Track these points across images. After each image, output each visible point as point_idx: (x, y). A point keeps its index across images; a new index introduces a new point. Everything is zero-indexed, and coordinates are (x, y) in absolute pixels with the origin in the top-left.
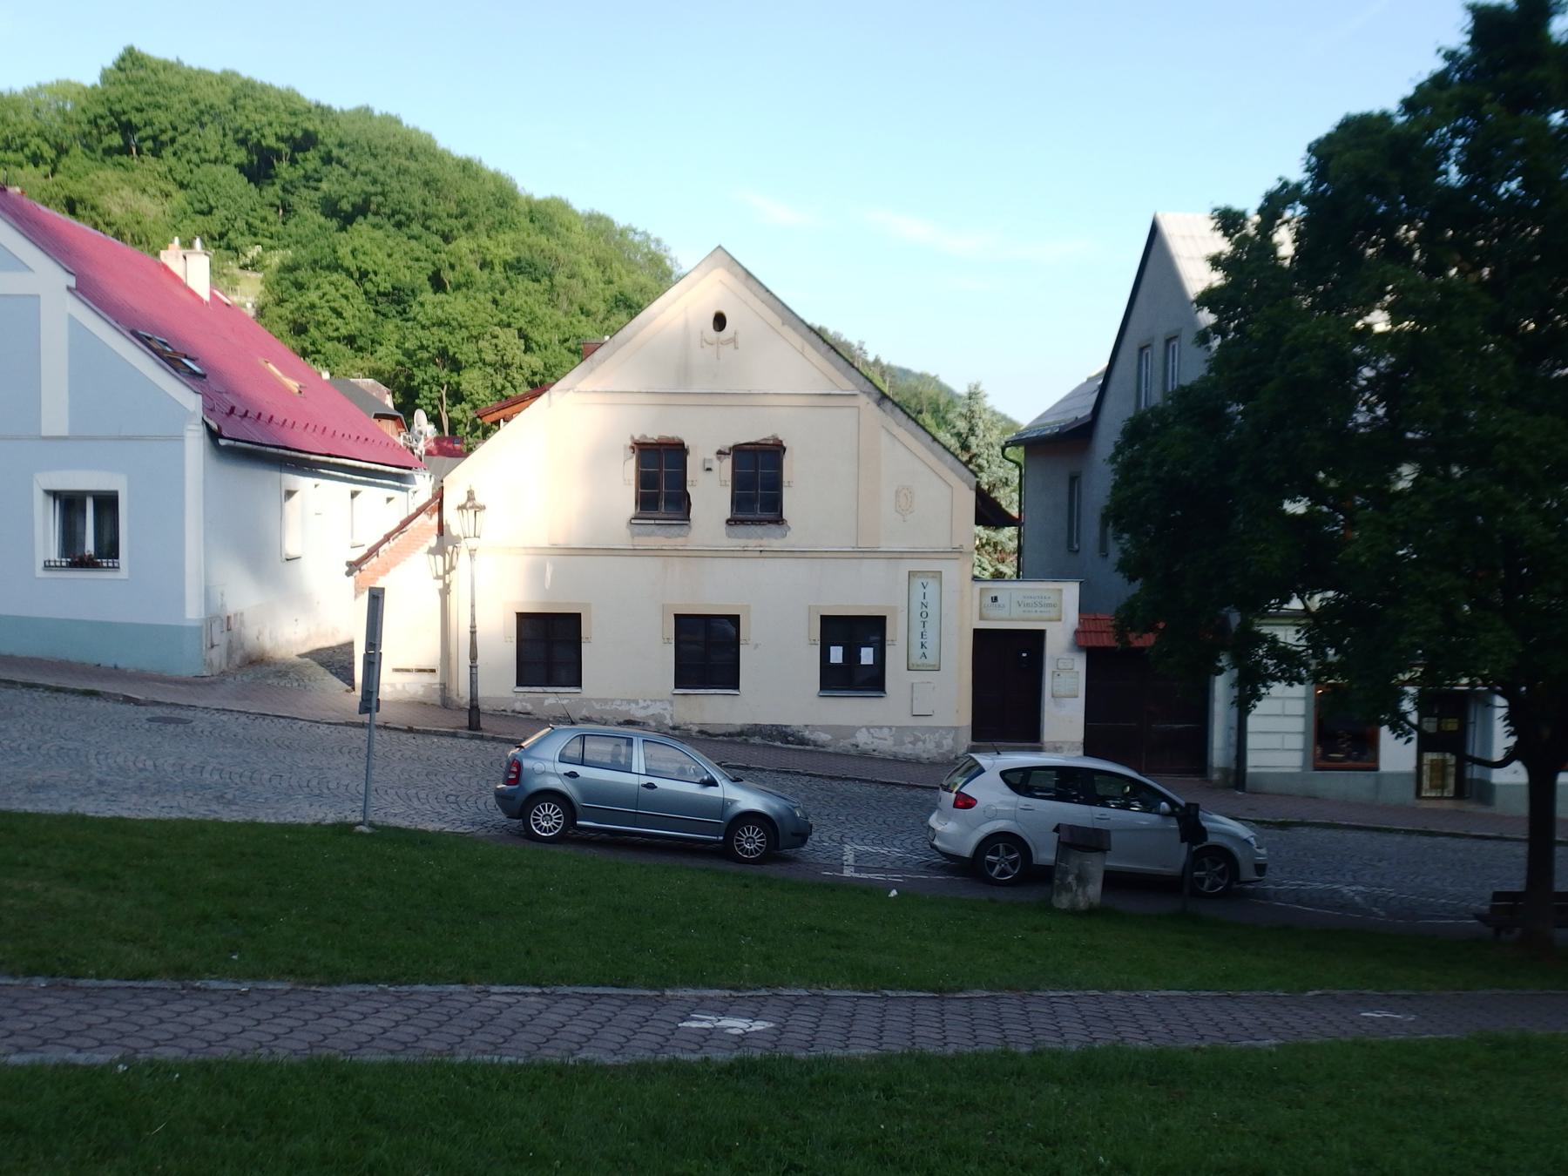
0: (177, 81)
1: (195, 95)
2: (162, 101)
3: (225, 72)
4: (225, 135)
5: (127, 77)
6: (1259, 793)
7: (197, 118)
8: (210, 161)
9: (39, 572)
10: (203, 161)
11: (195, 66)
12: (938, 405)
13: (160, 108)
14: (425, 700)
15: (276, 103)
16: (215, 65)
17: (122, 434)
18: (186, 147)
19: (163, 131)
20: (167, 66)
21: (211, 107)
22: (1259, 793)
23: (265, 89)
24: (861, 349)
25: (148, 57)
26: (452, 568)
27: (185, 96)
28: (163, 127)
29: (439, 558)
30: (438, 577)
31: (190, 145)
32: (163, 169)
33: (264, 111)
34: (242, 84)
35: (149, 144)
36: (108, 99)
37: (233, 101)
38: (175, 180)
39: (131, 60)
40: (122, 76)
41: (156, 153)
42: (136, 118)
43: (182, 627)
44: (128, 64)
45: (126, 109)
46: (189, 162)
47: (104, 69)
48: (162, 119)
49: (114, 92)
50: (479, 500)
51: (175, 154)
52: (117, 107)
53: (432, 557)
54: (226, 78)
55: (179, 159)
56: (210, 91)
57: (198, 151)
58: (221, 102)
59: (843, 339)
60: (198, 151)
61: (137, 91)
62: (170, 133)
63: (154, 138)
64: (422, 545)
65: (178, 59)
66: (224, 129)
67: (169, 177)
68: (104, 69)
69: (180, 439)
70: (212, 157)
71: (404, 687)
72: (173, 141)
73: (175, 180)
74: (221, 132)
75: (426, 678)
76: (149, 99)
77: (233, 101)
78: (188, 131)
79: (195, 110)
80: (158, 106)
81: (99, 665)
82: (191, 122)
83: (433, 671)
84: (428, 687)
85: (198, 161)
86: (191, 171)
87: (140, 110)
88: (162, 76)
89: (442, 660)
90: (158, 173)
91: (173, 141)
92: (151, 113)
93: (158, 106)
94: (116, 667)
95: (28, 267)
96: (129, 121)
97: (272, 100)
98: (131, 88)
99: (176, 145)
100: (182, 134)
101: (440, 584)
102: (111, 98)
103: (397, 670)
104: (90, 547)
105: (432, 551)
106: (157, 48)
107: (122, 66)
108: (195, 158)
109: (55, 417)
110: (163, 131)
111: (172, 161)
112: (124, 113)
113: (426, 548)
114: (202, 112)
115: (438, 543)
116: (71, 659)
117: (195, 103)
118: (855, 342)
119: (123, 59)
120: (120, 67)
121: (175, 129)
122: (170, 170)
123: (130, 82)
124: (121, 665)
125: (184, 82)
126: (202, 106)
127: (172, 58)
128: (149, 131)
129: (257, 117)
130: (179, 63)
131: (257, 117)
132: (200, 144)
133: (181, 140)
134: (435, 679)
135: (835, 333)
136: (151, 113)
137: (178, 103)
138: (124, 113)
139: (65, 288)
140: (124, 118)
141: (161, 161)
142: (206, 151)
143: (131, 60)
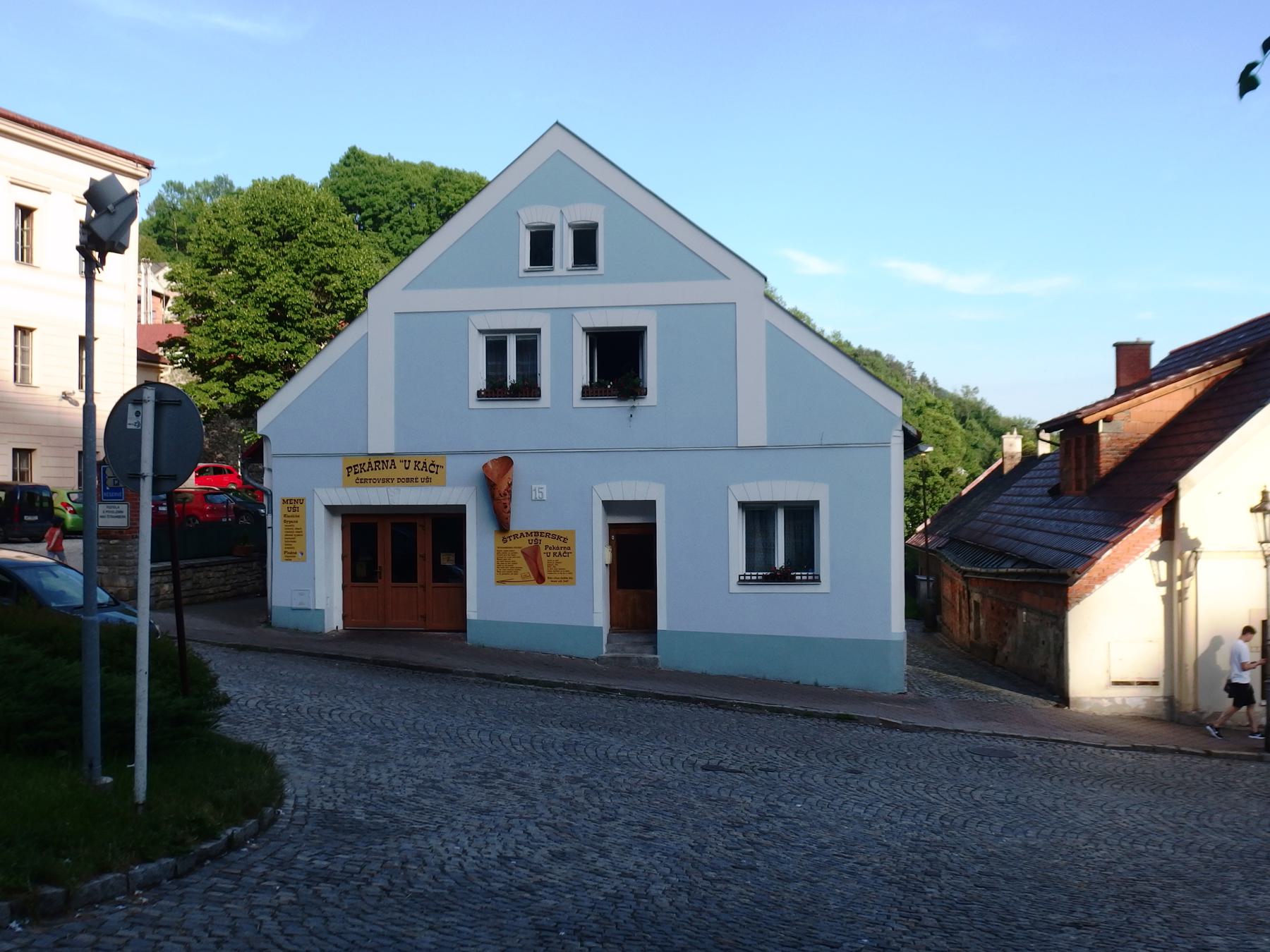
0: (390, 172)
1: (406, 182)
2: (380, 188)
3: (423, 163)
4: (429, 212)
5: (352, 170)
6: (229, 646)
7: (408, 200)
8: (420, 233)
9: (734, 587)
10: (414, 233)
11: (402, 160)
12: (980, 412)
13: (378, 193)
14: (1149, 714)
15: (470, 185)
16: (416, 158)
17: (824, 443)
18: (400, 222)
19: (382, 211)
20: (380, 161)
21: (419, 190)
22: (229, 646)
23: (460, 174)
24: (910, 368)
25: (368, 155)
26: (1186, 574)
27: (398, 183)
28: (382, 208)
29: (1163, 565)
30: (1160, 584)
31: (403, 221)
32: (382, 240)
33: (460, 191)
34: (441, 171)
35: (370, 222)
36: (338, 188)
37: (436, 185)
38: (391, 248)
39: (354, 157)
40: (348, 169)
41: (376, 228)
42: (360, 202)
43: (888, 642)
44: (352, 161)
45: (352, 195)
46: (402, 234)
47: (333, 166)
48: (381, 201)
49: (345, 182)
50: (1257, 501)
51: (391, 228)
52: (346, 194)
53: (1154, 562)
54: (426, 167)
55: (395, 232)
56: (415, 177)
57: (409, 225)
58: (426, 186)
59: (895, 360)
60: (409, 225)
61: (361, 181)
62: (387, 213)
63: (374, 217)
64: (1143, 551)
65: (389, 154)
66: (429, 207)
67: (387, 246)
68: (333, 166)
69: (886, 445)
70: (421, 229)
71: (1124, 700)
72: (388, 218)
73: (391, 248)
74: (427, 210)
75: (1148, 691)
76: (370, 187)
77: (436, 185)
78: (400, 211)
79: (406, 193)
80: (376, 192)
81: (798, 683)
82: (403, 203)
83: (1156, 683)
84: (1151, 700)
85: (410, 233)
86: (404, 241)
87: (363, 196)
88: (378, 168)
89: (1165, 671)
90: (379, 244)
91: (388, 218)
92: (372, 197)
93: (376, 192)
94: (816, 685)
95: (725, 276)
96: (354, 204)
97: (467, 182)
98: (356, 179)
99: (391, 222)
100: (397, 212)
101: (1163, 590)
102: (342, 187)
103: (1116, 683)
104: (780, 562)
105: (1155, 557)
106: (373, 147)
107: (348, 162)
108: (407, 231)
109: (753, 430)
110: (382, 211)
111: (390, 233)
112: (352, 198)
113: (1147, 553)
114: (411, 195)
115: (1161, 548)
116: (768, 677)
117: (407, 187)
118: (905, 363)
119: (348, 157)
120: (345, 162)
121: (391, 208)
122: (388, 242)
123: (354, 175)
124: (821, 682)
125: (395, 173)
126: (412, 190)
127: (384, 154)
128: (370, 212)
129: (457, 196)
130: (391, 157)
131: (457, 196)
132: (411, 219)
133: (398, 216)
134: (1158, 692)
135: (888, 355)
136: (372, 197)
137: (393, 188)
138: (352, 198)
139: (762, 294)
140: (350, 202)
141: (380, 234)
142: (416, 224)
143: (354, 157)
